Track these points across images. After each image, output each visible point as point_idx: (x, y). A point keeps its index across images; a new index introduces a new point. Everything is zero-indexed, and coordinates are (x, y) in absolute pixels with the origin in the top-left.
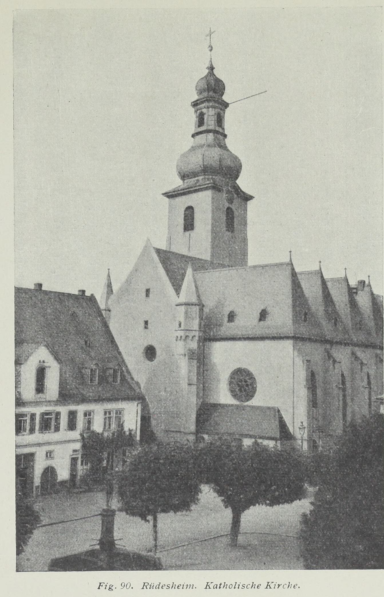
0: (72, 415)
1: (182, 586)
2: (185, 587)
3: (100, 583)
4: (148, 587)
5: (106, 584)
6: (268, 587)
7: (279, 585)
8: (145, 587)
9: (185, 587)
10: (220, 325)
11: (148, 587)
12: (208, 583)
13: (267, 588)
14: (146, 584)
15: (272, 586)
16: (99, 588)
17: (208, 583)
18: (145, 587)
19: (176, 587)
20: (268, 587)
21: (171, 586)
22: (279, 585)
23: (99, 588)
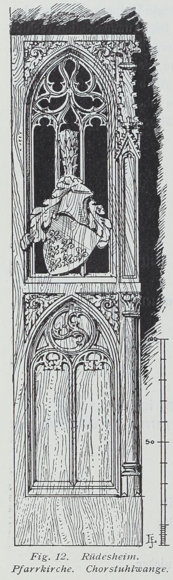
2: (126, 557)
4: (88, 558)
7: (52, 569)
8: (85, 558)
9: (126, 557)
11: (88, 558)
14: (86, 555)
16: (14, 571)
18: (85, 558)
19: (118, 557)
22: (52, 569)
23: (32, 559)
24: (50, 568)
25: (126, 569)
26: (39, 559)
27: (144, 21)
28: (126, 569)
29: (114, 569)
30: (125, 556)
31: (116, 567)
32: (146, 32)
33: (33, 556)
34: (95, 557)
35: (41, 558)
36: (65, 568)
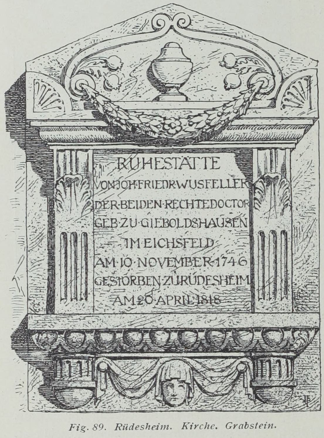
0: (273, 367)
1: (264, 426)
2: (267, 426)
3: (72, 425)
4: (122, 428)
5: (78, 425)
6: (185, 427)
7: (196, 426)
8: (118, 428)
9: (267, 426)
10: (259, 394)
11: (122, 428)
12: (185, 423)
13: (183, 429)
14: (119, 425)
15: (189, 426)
16: (70, 430)
17: (185, 423)
18: (118, 428)
19: (210, 427)
20: (185, 427)
21: (145, 427)
22: (196, 426)
23: (70, 430)
24: (267, 424)
25: (147, 427)
26: (77, 430)
27: (10, 337)
28: (147, 427)
29: (254, 426)
30: (158, 426)
31: (257, 424)
32: (103, 121)
33: (72, 427)
34: (128, 428)
35: (80, 428)
36: (149, 426)
